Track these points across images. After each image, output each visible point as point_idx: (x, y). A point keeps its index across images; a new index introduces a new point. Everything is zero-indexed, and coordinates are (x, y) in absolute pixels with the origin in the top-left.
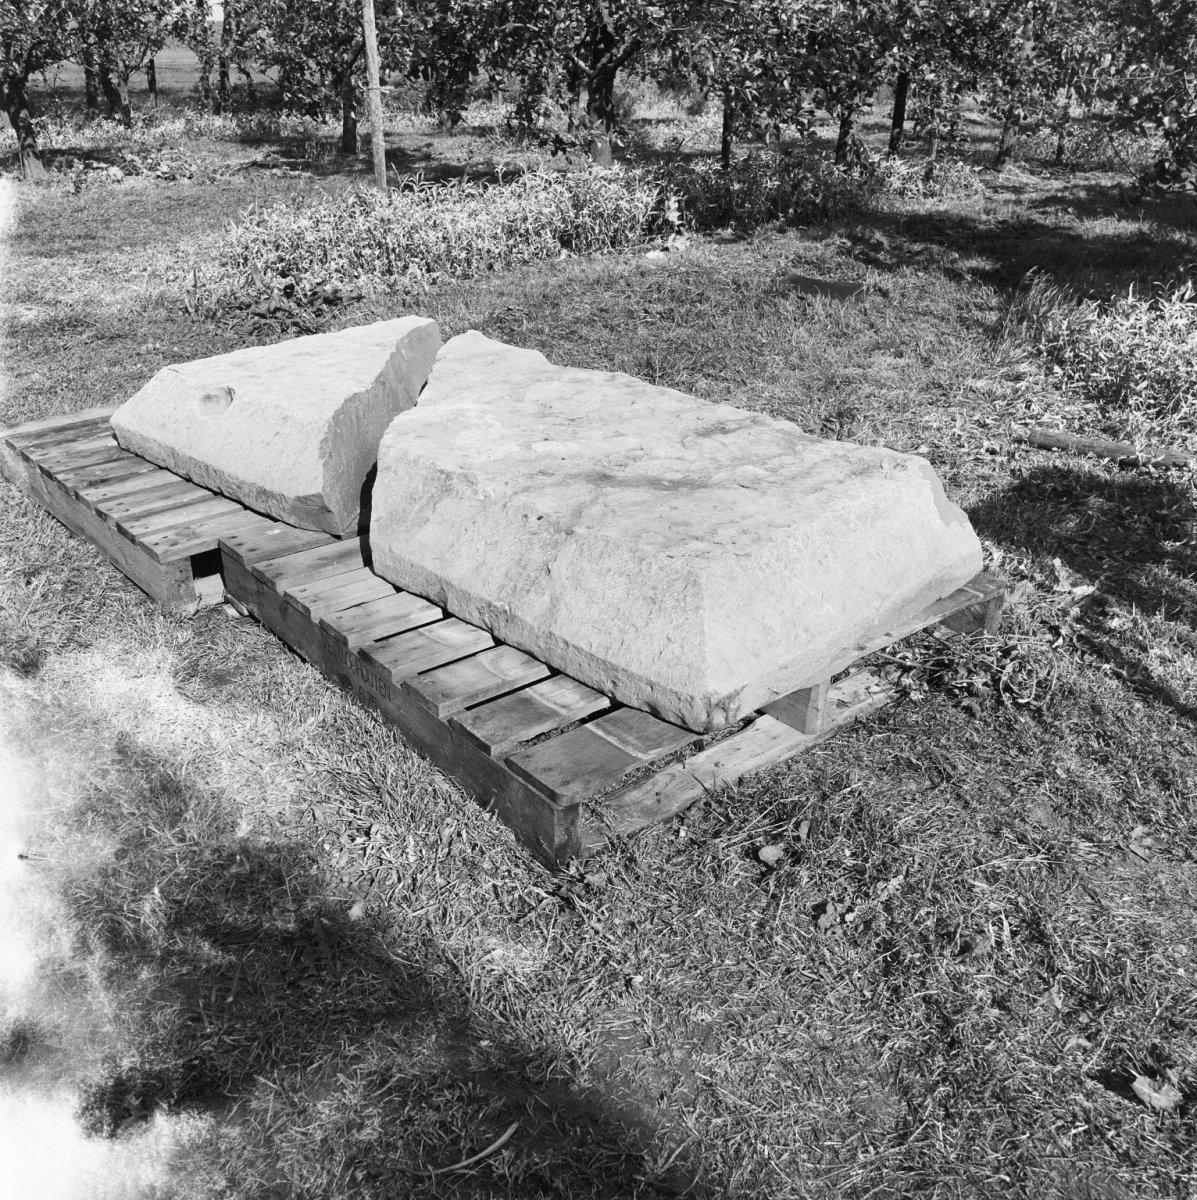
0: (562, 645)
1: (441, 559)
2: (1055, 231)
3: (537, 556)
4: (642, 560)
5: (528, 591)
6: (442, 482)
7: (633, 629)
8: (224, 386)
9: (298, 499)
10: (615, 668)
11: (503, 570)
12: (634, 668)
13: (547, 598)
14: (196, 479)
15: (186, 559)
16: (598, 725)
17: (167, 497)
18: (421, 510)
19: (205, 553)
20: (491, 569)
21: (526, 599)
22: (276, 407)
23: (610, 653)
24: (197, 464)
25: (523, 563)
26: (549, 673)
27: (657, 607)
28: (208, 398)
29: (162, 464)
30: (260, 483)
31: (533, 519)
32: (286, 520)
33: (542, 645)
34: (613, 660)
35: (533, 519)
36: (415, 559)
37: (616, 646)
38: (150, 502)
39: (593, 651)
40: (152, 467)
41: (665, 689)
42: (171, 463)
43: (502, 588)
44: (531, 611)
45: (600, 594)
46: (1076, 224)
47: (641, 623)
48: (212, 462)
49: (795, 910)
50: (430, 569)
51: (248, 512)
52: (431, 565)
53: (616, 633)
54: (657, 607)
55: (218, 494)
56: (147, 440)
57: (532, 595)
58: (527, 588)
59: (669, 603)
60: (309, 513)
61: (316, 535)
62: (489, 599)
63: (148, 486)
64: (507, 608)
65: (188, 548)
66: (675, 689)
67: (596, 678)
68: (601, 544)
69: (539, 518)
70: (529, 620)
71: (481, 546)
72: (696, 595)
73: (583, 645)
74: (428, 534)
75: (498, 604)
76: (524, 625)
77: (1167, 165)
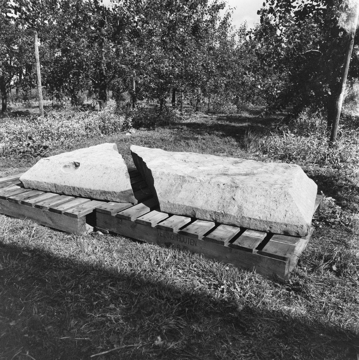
0: (248, 219)
1: (191, 202)
2: (227, 125)
3: (228, 196)
4: (267, 191)
5: (229, 206)
6: (182, 179)
7: (272, 210)
8: (73, 162)
9: (122, 192)
10: (271, 222)
11: (217, 201)
12: (278, 221)
13: (236, 207)
14: (67, 193)
15: (84, 216)
16: (256, 240)
17: (60, 200)
20: (212, 202)
21: (229, 208)
22: (101, 165)
23: (268, 218)
24: (69, 187)
25: (223, 198)
27: (278, 202)
28: (65, 166)
30: (102, 189)
31: (221, 185)
32: (114, 200)
33: (239, 221)
34: (270, 220)
36: (180, 203)
37: (269, 216)
38: (55, 202)
40: (43, 192)
41: (291, 225)
42: (54, 189)
43: (218, 207)
44: (233, 211)
45: (256, 202)
46: (230, 124)
47: (275, 208)
48: (77, 185)
50: (187, 205)
51: (93, 201)
52: (187, 204)
53: (267, 212)
54: (278, 202)
56: (41, 183)
57: (231, 207)
58: (228, 205)
59: (282, 201)
60: (124, 197)
61: (127, 204)
62: (215, 210)
63: (49, 197)
64: (223, 212)
65: (85, 212)
66: (295, 224)
67: (263, 227)
68: (250, 189)
69: (224, 185)
70: (233, 214)
71: (205, 195)
72: (290, 197)
73: (257, 218)
74: (183, 194)
75: (219, 211)
76: (231, 216)
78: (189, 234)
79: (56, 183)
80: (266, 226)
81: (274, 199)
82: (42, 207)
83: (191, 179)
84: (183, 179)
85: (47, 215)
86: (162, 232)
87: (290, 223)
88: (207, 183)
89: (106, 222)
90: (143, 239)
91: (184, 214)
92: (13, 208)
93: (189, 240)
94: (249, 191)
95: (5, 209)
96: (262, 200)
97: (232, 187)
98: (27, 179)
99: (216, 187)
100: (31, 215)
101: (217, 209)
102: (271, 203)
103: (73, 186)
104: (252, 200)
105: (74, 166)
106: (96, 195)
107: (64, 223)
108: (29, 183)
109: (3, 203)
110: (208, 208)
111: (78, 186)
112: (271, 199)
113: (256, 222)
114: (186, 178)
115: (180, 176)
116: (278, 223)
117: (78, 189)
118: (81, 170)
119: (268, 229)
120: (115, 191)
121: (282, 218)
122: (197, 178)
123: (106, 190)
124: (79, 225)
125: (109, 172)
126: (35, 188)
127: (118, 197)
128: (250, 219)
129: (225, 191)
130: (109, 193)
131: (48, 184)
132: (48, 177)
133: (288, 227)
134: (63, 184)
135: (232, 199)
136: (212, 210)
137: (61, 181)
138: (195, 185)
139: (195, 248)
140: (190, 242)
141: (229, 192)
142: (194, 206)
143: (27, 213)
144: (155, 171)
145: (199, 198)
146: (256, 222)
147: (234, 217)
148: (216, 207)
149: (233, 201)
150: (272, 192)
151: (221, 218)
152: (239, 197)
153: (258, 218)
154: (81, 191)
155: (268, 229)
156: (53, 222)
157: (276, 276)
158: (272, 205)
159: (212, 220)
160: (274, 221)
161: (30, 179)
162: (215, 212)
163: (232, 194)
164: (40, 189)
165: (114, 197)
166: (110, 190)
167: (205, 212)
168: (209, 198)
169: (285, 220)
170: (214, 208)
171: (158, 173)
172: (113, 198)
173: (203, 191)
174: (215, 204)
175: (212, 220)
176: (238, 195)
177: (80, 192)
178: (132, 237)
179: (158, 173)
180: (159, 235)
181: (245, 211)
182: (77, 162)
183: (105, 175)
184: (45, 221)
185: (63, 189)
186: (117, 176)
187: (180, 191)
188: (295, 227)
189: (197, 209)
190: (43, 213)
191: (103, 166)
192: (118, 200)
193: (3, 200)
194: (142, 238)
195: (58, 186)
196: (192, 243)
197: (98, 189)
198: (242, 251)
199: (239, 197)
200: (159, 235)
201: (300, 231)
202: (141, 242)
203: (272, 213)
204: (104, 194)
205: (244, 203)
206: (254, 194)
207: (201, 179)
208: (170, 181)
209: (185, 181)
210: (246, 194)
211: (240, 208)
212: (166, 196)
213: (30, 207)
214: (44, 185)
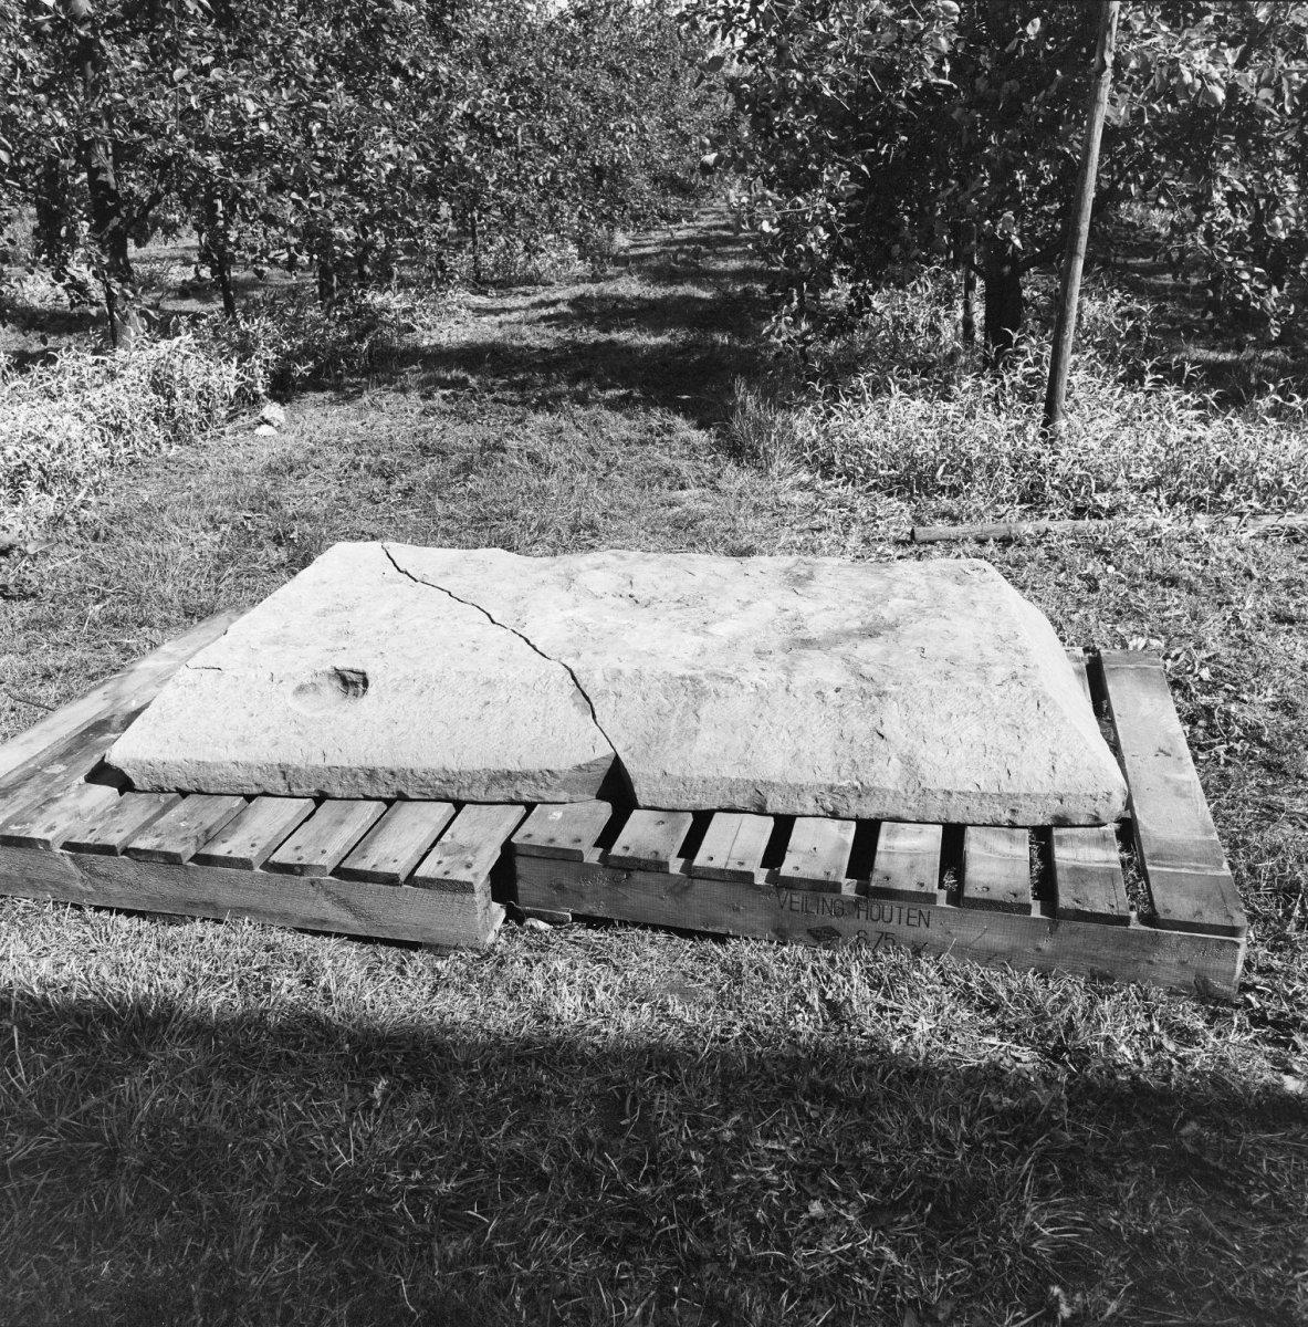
3: (860, 726)
6: (690, 688)
8: (328, 668)
10: (1012, 796)
11: (828, 750)
12: (1036, 789)
13: (894, 760)
18: (681, 722)
19: (699, 844)
24: (344, 772)
26: (419, 873)
29: (255, 790)
30: (493, 766)
31: (830, 693)
32: (548, 799)
33: (914, 805)
34: (1011, 790)
35: (830, 693)
36: (709, 773)
39: (984, 788)
41: (1077, 796)
45: (955, 738)
48: (382, 761)
49: (216, 74)
52: (731, 772)
55: (184, 794)
59: (1033, 723)
64: (857, 783)
69: (837, 690)
70: (891, 786)
72: (1054, 708)
74: (706, 742)
75: (844, 784)
76: (884, 792)
77: (1208, 215)
78: (903, 892)
79: (285, 760)
80: (999, 810)
81: (1008, 721)
82: (302, 866)
83: (722, 686)
84: (693, 688)
85: (328, 893)
86: (795, 898)
87: (1074, 792)
88: (781, 690)
89: (560, 888)
90: (721, 924)
91: (726, 806)
92: (156, 884)
93: (904, 911)
94: (924, 702)
95: (115, 888)
96: (974, 730)
97: (864, 694)
98: (147, 757)
99: (814, 703)
100: (253, 899)
101: (836, 777)
102: (1002, 733)
103: (369, 764)
104: (939, 731)
105: (337, 683)
106: (470, 787)
107: (411, 913)
108: (159, 770)
109: (100, 869)
110: (806, 777)
111: (388, 765)
112: (1000, 719)
113: (967, 802)
114: (706, 682)
115: (683, 678)
116: (1037, 795)
117: (392, 773)
118: (381, 700)
119: (1008, 815)
120: (552, 768)
121: (1046, 779)
122: (744, 679)
123: (513, 766)
124: (479, 908)
125: (503, 696)
126: (185, 786)
127: (564, 787)
128: (949, 793)
129: (845, 712)
130: (526, 775)
131: (248, 767)
132: (243, 740)
133: (1066, 803)
134: (318, 761)
135: (876, 737)
136: (821, 780)
137: (306, 752)
138: (741, 704)
139: (923, 932)
140: (904, 918)
141: (860, 714)
142: (758, 777)
143: (226, 896)
144: (588, 671)
145: (766, 746)
146: (967, 802)
147: (896, 794)
148: (830, 770)
149: (880, 744)
150: (996, 698)
151: (853, 802)
152: (896, 728)
153: (974, 789)
154: (405, 779)
155: (1008, 815)
156: (357, 915)
157: (1205, 982)
158: (1006, 740)
159: (821, 812)
160: (1024, 791)
161: (161, 758)
162: (831, 788)
163: (874, 721)
164: (212, 791)
165: (549, 787)
166: (532, 764)
167: (799, 790)
168: (802, 744)
169: (1057, 781)
170: (827, 776)
171: (598, 676)
172: (542, 793)
173: (774, 720)
174: (826, 761)
175: (821, 812)
176: (893, 718)
177: (397, 785)
178: (672, 924)
179: (598, 676)
180: (786, 907)
181: (926, 769)
182: (349, 667)
183: (490, 709)
184: (316, 914)
185: (322, 781)
186: (540, 709)
187: (696, 732)
188: (1089, 801)
189: (769, 785)
190: (311, 890)
191: (469, 677)
192: (563, 796)
193: (102, 858)
194: (715, 924)
195: (297, 770)
196: (912, 921)
197: (477, 766)
198: (1093, 926)
199: (896, 728)
200: (786, 907)
201: (1102, 811)
202: (720, 939)
203: (1012, 765)
204: (504, 783)
205: (917, 744)
206: (942, 710)
207: (756, 679)
208: (651, 701)
209: (702, 694)
210: (918, 716)
211: (908, 761)
212: (652, 754)
213: (244, 872)
214: (229, 775)
